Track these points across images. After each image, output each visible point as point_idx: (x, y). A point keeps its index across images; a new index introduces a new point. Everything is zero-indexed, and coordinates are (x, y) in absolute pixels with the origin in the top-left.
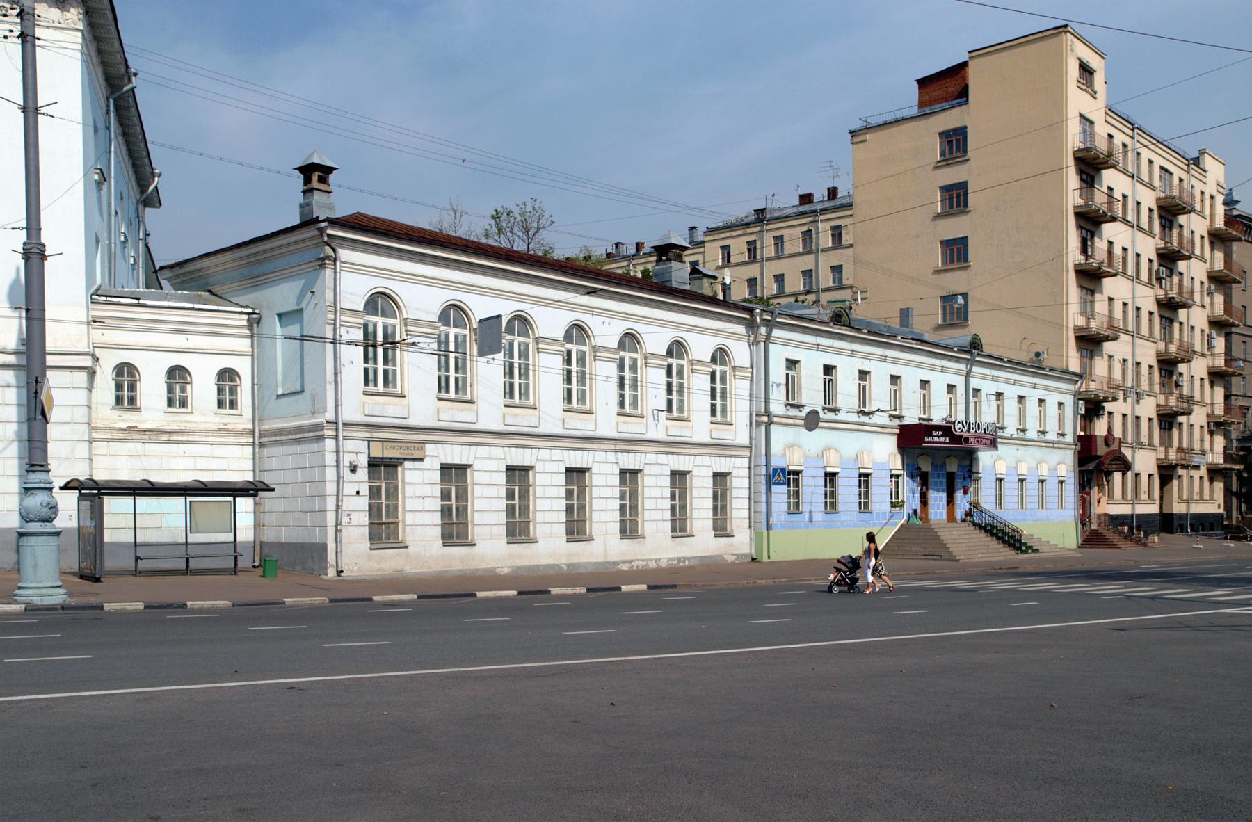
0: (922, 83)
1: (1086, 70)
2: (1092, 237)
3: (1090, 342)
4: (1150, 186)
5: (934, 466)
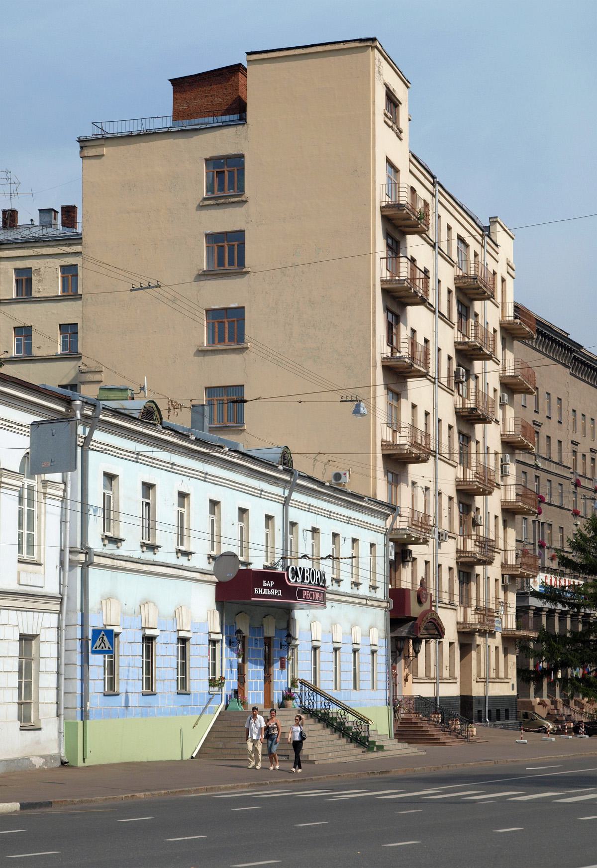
0: (178, 84)
1: (392, 101)
2: (398, 322)
3: (397, 462)
4: (451, 263)
5: (252, 628)
